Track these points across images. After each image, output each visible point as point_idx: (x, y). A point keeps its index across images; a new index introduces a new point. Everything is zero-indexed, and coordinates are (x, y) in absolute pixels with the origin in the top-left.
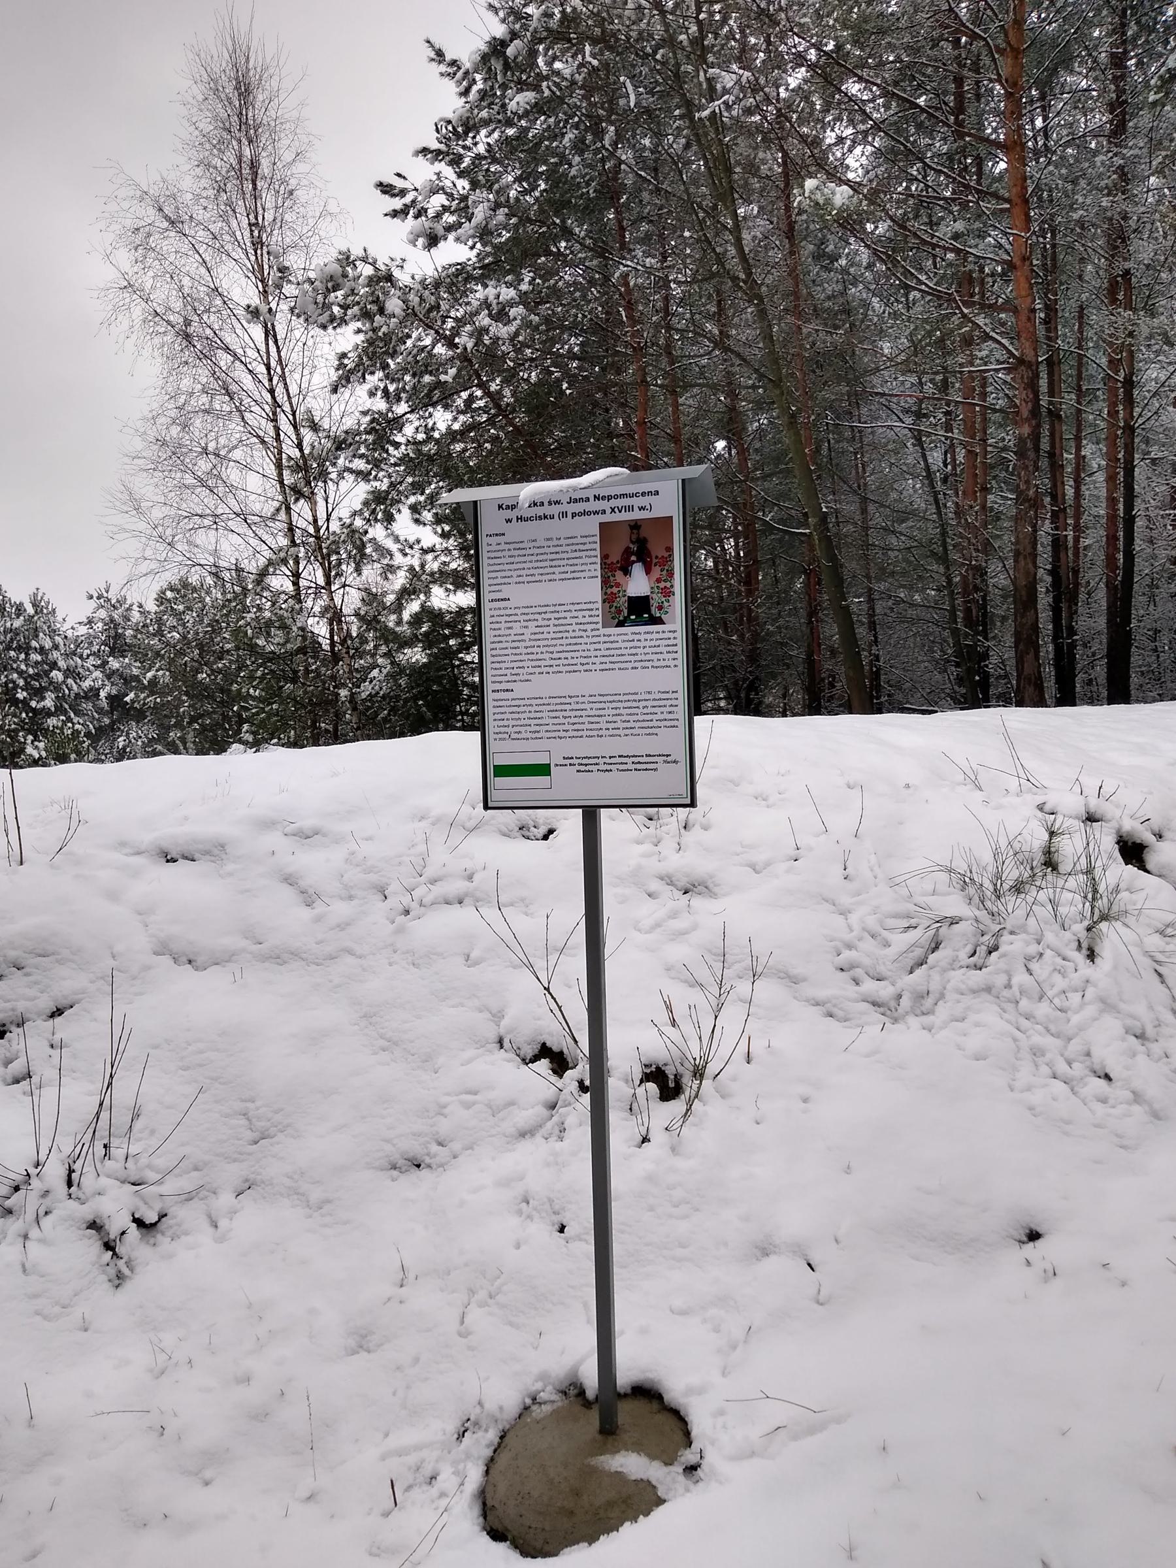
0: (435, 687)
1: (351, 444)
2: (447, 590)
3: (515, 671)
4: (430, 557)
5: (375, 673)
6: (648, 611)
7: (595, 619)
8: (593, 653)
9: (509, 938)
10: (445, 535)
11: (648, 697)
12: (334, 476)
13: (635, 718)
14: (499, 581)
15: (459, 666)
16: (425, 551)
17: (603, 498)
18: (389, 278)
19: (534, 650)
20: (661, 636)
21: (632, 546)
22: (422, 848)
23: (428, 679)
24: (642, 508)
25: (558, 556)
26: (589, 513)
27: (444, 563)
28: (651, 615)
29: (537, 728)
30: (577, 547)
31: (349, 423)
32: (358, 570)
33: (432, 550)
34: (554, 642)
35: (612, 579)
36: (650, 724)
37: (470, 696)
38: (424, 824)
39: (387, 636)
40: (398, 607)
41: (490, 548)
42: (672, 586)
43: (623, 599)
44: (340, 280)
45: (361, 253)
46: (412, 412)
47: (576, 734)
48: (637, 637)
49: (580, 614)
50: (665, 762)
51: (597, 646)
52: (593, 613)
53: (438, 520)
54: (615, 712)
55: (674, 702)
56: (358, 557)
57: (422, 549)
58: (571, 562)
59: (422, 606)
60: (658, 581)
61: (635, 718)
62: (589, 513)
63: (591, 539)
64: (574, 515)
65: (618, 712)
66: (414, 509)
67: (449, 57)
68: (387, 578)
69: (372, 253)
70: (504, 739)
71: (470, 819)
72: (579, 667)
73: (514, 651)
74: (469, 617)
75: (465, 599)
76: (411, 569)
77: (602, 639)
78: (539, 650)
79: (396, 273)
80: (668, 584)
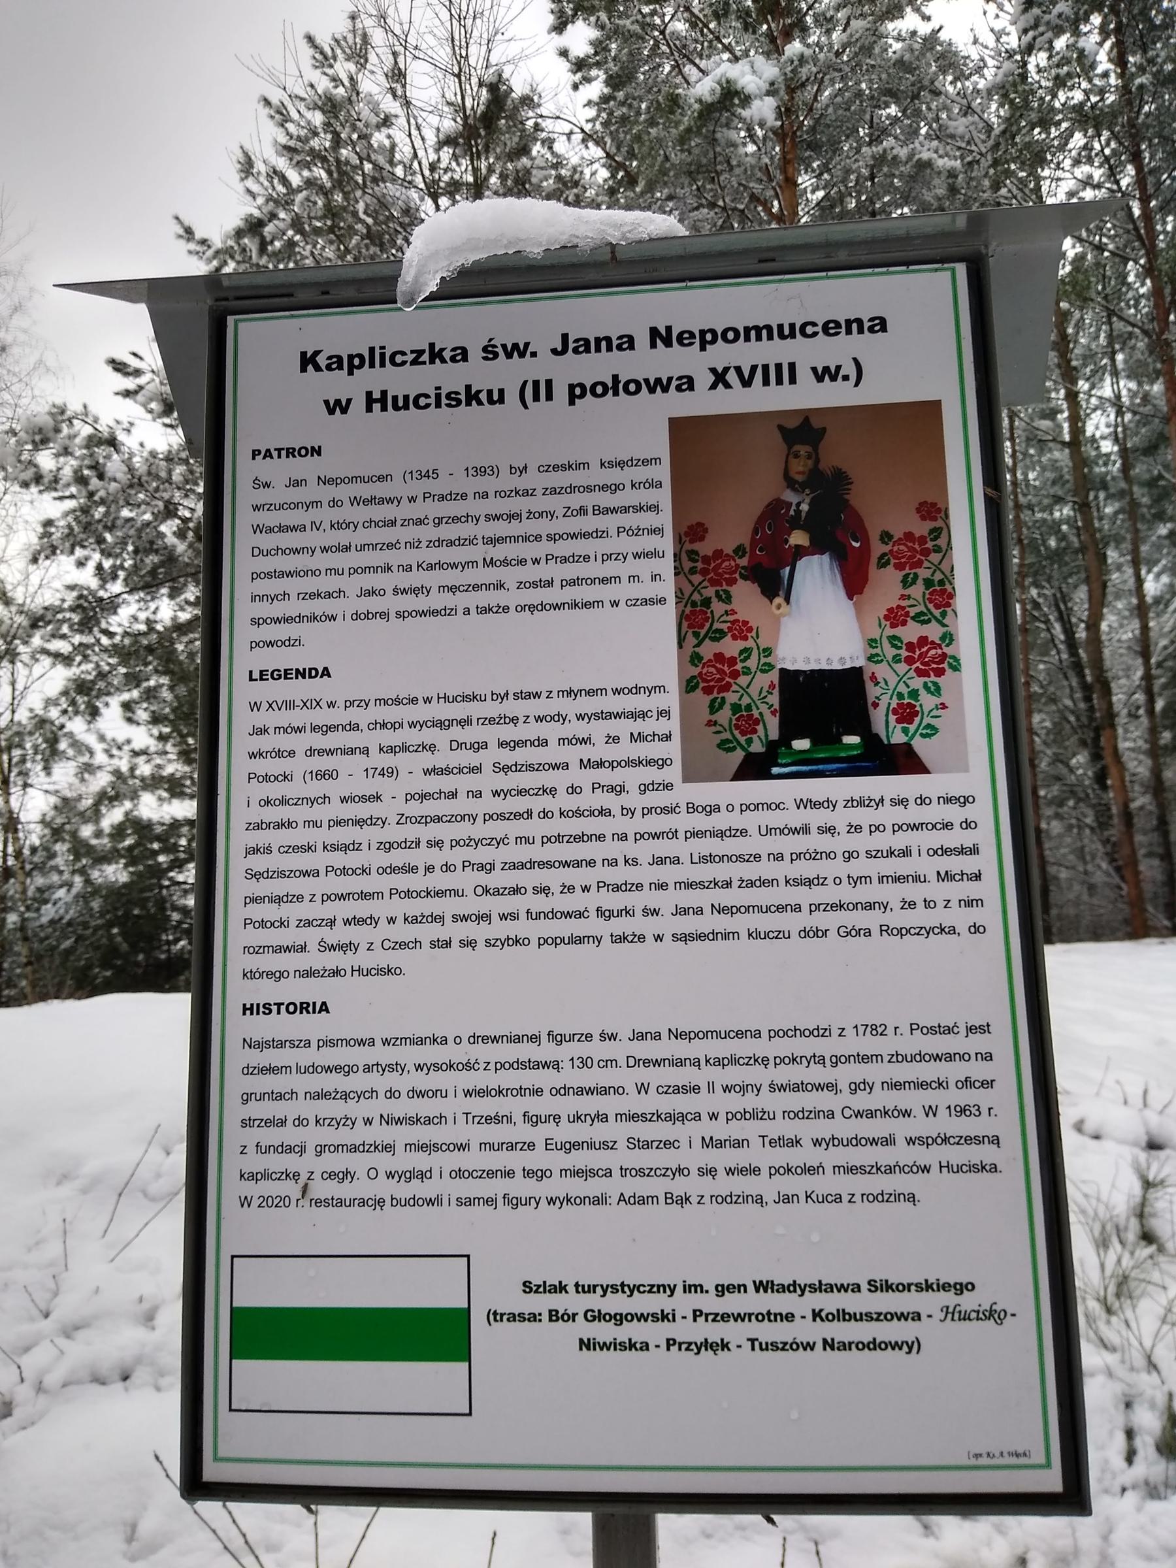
0: (136, 912)
1: (50, 622)
2: (160, 799)
3: (340, 934)
4: (141, 760)
5: (61, 893)
6: (862, 725)
7: (655, 750)
8: (645, 874)
9: (237, 1543)
10: (162, 738)
11: (869, 1044)
12: (25, 658)
13: (823, 1128)
14: (292, 607)
15: (168, 887)
16: (136, 754)
17: (685, 339)
18: (112, 442)
19: (418, 857)
20: (914, 814)
21: (791, 497)
22: (54, 1249)
23: (129, 901)
24: (824, 374)
25: (515, 528)
26: (633, 387)
27: (159, 767)
28: (871, 740)
29: (421, 1161)
30: (588, 500)
31: (49, 598)
32: (47, 769)
33: (144, 752)
34: (497, 829)
35: (718, 607)
36: (884, 1156)
37: (180, 922)
38: (66, 1190)
39: (80, 848)
40: (94, 814)
41: (263, 496)
42: (949, 638)
43: (764, 680)
44: (51, 434)
45: (79, 408)
46: (130, 592)
47: (577, 1187)
48: (816, 818)
49: (599, 729)
50: (950, 1313)
51: (663, 848)
52: (647, 726)
53: (156, 720)
54: (735, 1102)
55: (978, 1070)
56: (48, 752)
57: (133, 751)
58: (565, 548)
59: (127, 814)
60: (896, 617)
61: (823, 1128)
62: (633, 387)
63: (641, 474)
64: (576, 393)
65: (750, 1102)
66: (127, 706)
67: (199, 235)
68: (83, 780)
69: (93, 409)
70: (282, 1202)
71: (158, 1176)
72: (593, 925)
73: (339, 859)
74: (185, 830)
75: (186, 809)
76: (117, 773)
77: (683, 822)
78: (436, 857)
79: (121, 437)
80: (933, 631)
